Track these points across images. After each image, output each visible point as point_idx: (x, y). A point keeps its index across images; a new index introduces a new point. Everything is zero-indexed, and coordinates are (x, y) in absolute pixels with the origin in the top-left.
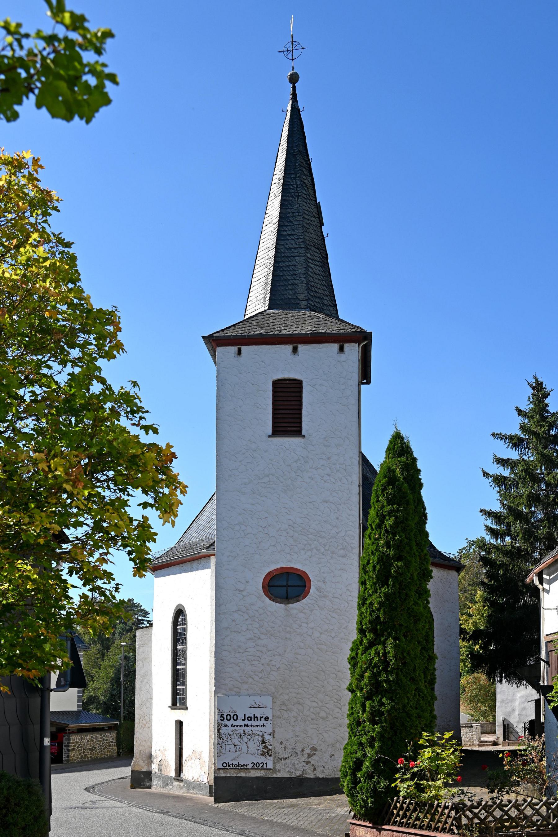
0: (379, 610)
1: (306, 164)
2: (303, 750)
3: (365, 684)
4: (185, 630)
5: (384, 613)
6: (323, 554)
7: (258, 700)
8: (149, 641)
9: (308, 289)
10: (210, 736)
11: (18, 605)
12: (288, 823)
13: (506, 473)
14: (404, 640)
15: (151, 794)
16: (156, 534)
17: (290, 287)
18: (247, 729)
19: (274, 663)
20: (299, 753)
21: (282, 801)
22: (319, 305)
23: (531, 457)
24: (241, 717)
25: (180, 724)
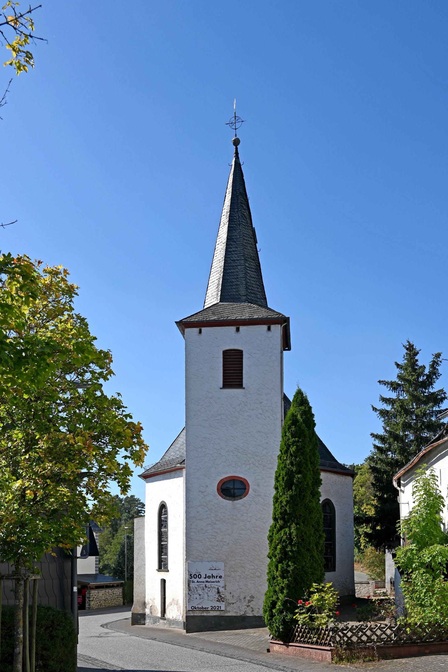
0: (286, 505)
1: (245, 201)
2: (245, 598)
3: (278, 553)
4: (166, 518)
5: (290, 508)
6: (257, 467)
7: (215, 564)
8: (142, 526)
9: (247, 287)
10: (184, 589)
11: (60, 510)
12: (233, 644)
13: (388, 408)
14: (302, 524)
15: (145, 628)
16: (133, 472)
17: (234, 287)
18: (208, 584)
19: (225, 540)
20: (243, 600)
21: (231, 631)
22: (254, 299)
23: (405, 396)
24: (203, 576)
25: (164, 582)
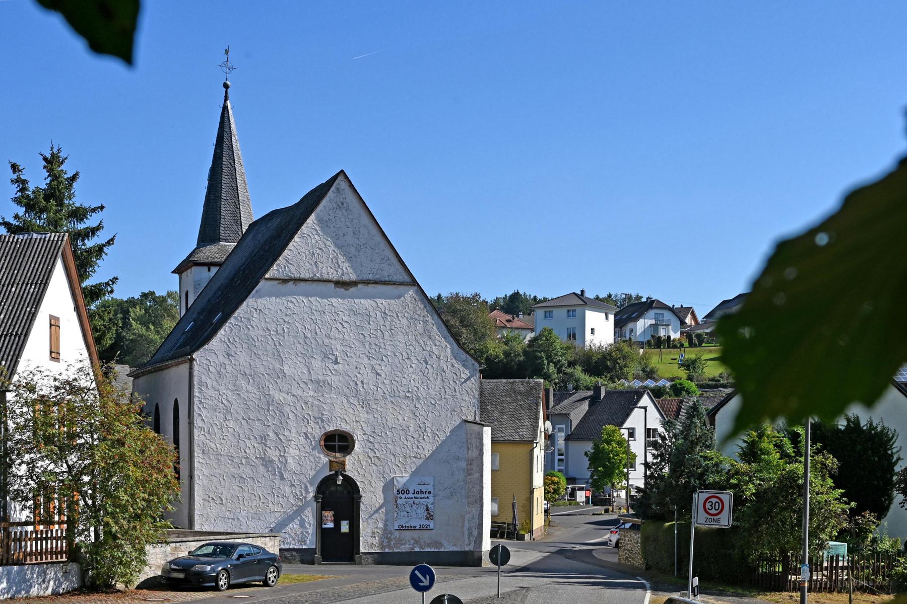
18: (416, 501)
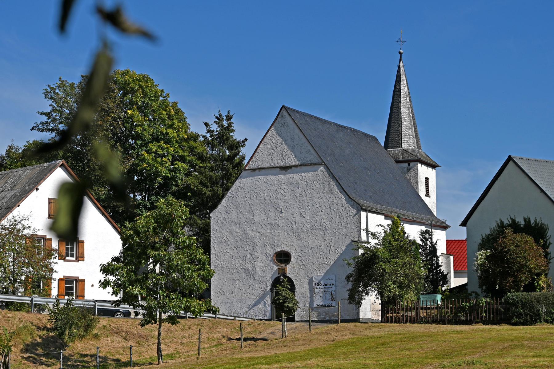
24: (323, 284)
